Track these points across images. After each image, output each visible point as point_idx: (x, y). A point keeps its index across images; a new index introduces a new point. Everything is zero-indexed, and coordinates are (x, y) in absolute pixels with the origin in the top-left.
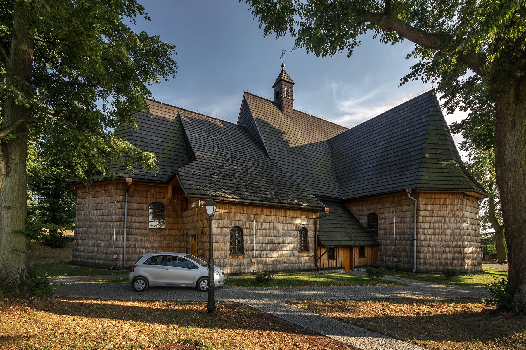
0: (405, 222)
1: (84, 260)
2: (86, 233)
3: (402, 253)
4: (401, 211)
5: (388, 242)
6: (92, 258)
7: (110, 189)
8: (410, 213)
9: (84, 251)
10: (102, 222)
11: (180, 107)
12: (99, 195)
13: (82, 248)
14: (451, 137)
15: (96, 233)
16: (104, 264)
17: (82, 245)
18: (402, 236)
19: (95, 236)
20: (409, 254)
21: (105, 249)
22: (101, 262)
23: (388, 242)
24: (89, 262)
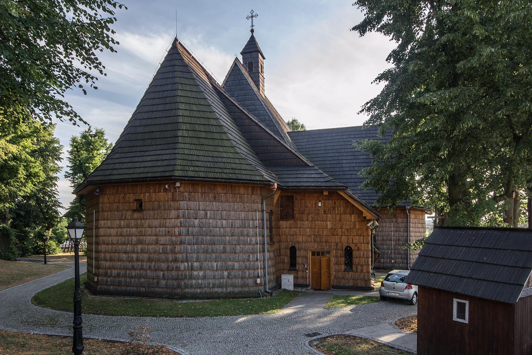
0: (400, 231)
1: (207, 290)
2: (206, 252)
3: (397, 256)
4: (396, 222)
5: (385, 246)
6: (220, 286)
7: (242, 192)
8: (404, 224)
9: (204, 277)
10: (232, 236)
11: (198, 61)
12: (223, 199)
13: (201, 273)
14: (226, 82)
15: (224, 252)
16: (240, 292)
17: (201, 269)
18: (397, 242)
19: (223, 256)
20: (403, 256)
21: (240, 273)
22: (236, 290)
23: (385, 246)
24: (216, 292)
